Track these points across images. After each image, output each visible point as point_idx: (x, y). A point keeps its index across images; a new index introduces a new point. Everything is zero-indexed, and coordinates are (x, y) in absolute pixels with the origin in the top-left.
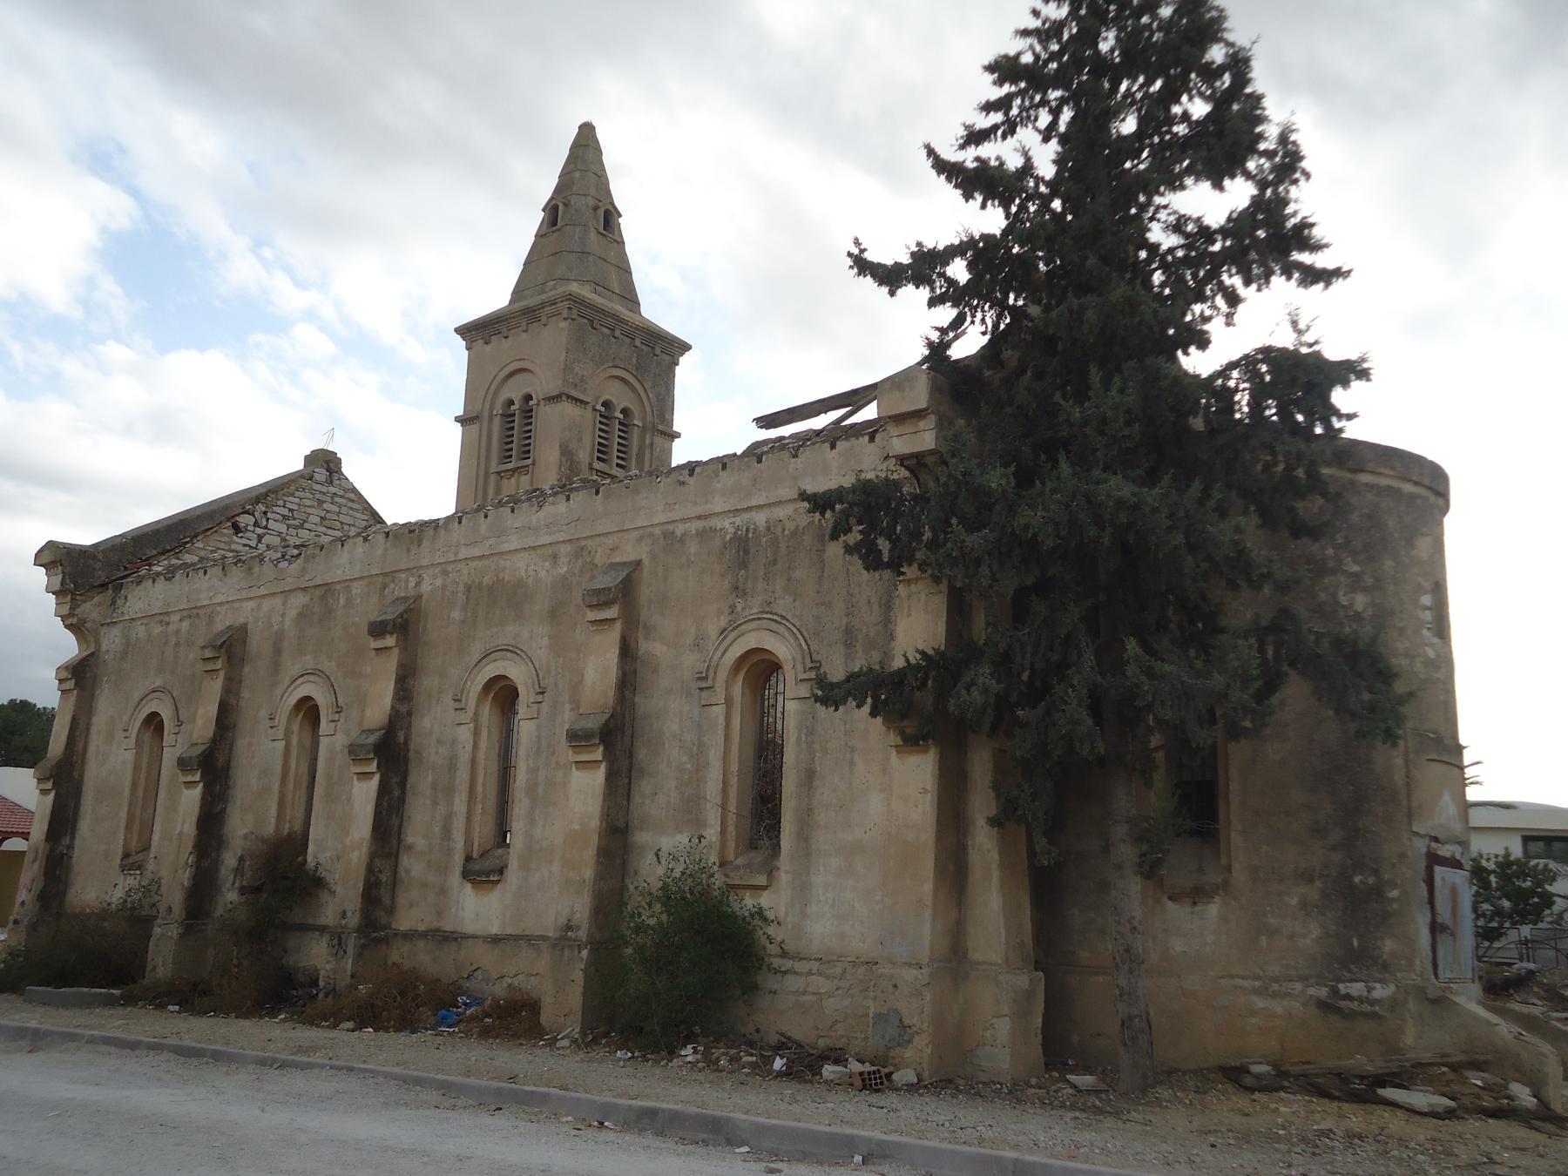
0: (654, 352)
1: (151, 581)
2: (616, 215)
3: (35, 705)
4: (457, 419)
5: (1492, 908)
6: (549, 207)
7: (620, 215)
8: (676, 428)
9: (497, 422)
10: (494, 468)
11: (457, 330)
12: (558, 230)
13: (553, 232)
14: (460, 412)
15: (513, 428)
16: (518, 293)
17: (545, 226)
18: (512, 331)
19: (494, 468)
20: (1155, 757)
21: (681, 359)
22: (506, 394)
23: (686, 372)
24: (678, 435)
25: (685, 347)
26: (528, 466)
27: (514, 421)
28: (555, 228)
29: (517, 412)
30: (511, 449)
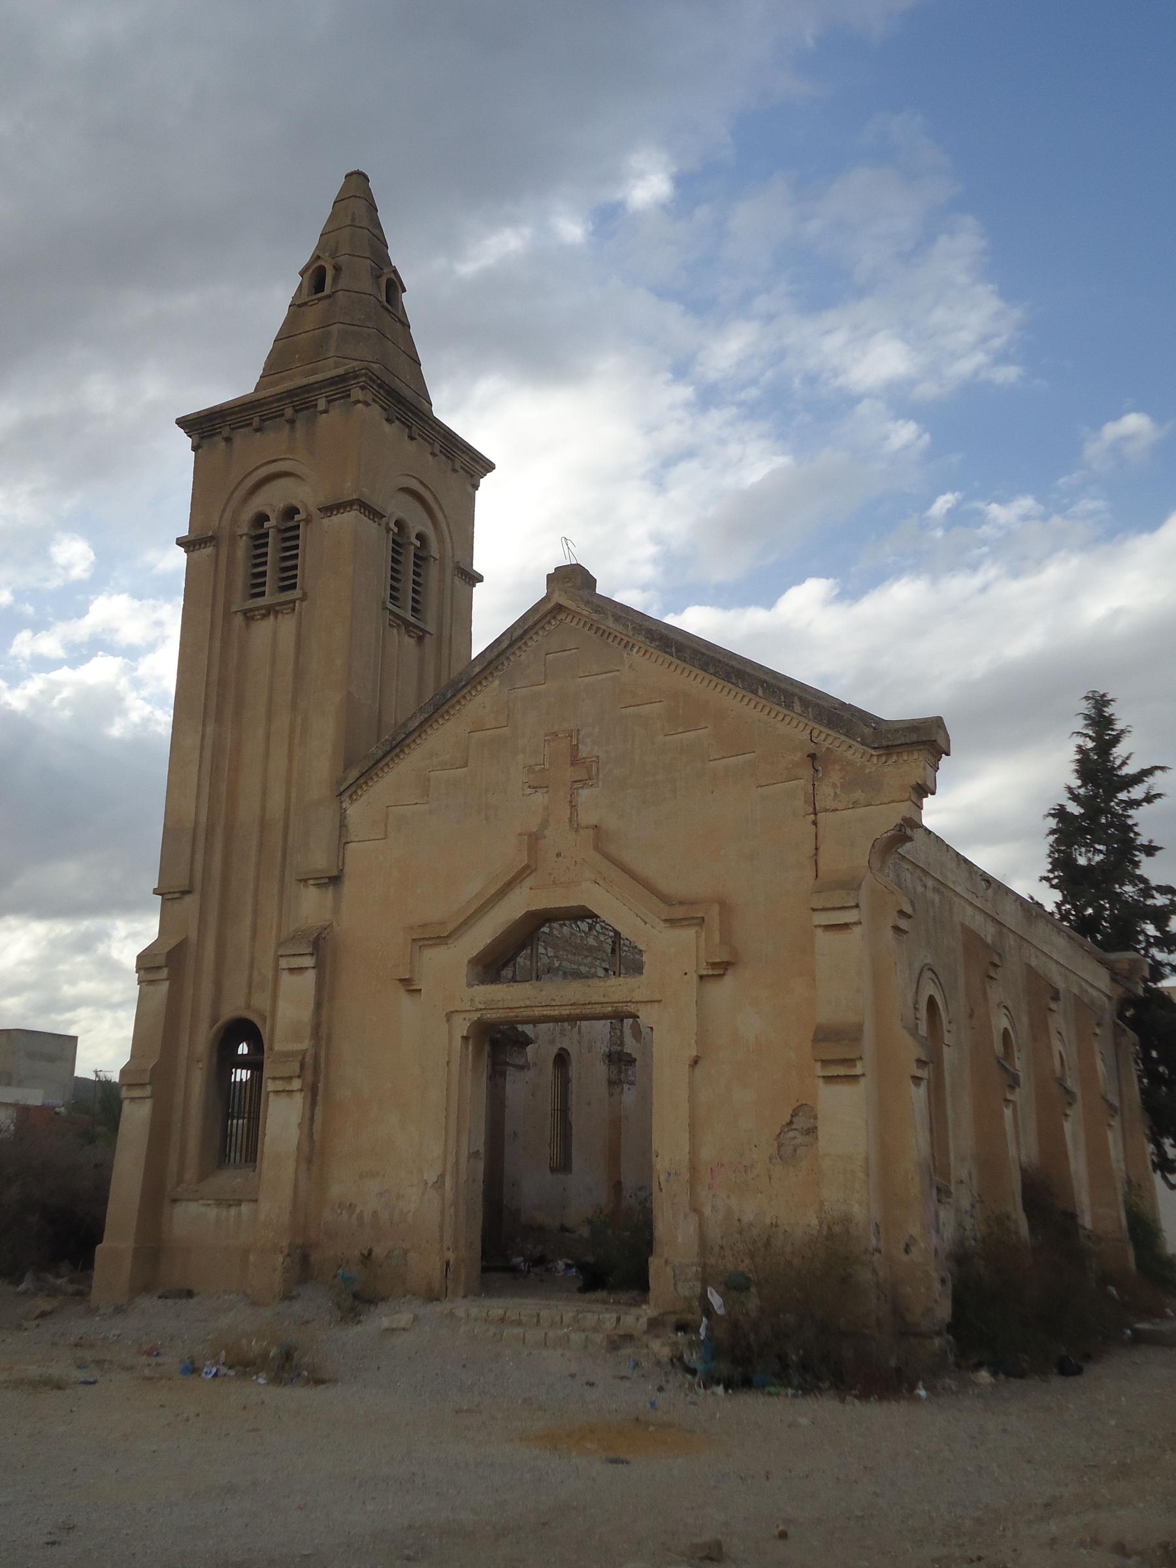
0: (453, 466)
1: (924, 1059)
2: (400, 290)
3: (1078, 805)
4: (181, 542)
5: (1158, 934)
6: (313, 268)
7: (404, 290)
8: (478, 566)
9: (243, 543)
10: (239, 604)
11: (183, 423)
12: (329, 297)
13: (319, 299)
14: (184, 532)
15: (264, 574)
16: (276, 365)
17: (305, 291)
18: (268, 422)
19: (239, 604)
20: (308, 948)
21: (482, 481)
22: (259, 503)
23: (487, 493)
24: (480, 579)
25: (489, 467)
26: (294, 601)
27: (266, 554)
28: (320, 295)
29: (271, 531)
30: (264, 574)
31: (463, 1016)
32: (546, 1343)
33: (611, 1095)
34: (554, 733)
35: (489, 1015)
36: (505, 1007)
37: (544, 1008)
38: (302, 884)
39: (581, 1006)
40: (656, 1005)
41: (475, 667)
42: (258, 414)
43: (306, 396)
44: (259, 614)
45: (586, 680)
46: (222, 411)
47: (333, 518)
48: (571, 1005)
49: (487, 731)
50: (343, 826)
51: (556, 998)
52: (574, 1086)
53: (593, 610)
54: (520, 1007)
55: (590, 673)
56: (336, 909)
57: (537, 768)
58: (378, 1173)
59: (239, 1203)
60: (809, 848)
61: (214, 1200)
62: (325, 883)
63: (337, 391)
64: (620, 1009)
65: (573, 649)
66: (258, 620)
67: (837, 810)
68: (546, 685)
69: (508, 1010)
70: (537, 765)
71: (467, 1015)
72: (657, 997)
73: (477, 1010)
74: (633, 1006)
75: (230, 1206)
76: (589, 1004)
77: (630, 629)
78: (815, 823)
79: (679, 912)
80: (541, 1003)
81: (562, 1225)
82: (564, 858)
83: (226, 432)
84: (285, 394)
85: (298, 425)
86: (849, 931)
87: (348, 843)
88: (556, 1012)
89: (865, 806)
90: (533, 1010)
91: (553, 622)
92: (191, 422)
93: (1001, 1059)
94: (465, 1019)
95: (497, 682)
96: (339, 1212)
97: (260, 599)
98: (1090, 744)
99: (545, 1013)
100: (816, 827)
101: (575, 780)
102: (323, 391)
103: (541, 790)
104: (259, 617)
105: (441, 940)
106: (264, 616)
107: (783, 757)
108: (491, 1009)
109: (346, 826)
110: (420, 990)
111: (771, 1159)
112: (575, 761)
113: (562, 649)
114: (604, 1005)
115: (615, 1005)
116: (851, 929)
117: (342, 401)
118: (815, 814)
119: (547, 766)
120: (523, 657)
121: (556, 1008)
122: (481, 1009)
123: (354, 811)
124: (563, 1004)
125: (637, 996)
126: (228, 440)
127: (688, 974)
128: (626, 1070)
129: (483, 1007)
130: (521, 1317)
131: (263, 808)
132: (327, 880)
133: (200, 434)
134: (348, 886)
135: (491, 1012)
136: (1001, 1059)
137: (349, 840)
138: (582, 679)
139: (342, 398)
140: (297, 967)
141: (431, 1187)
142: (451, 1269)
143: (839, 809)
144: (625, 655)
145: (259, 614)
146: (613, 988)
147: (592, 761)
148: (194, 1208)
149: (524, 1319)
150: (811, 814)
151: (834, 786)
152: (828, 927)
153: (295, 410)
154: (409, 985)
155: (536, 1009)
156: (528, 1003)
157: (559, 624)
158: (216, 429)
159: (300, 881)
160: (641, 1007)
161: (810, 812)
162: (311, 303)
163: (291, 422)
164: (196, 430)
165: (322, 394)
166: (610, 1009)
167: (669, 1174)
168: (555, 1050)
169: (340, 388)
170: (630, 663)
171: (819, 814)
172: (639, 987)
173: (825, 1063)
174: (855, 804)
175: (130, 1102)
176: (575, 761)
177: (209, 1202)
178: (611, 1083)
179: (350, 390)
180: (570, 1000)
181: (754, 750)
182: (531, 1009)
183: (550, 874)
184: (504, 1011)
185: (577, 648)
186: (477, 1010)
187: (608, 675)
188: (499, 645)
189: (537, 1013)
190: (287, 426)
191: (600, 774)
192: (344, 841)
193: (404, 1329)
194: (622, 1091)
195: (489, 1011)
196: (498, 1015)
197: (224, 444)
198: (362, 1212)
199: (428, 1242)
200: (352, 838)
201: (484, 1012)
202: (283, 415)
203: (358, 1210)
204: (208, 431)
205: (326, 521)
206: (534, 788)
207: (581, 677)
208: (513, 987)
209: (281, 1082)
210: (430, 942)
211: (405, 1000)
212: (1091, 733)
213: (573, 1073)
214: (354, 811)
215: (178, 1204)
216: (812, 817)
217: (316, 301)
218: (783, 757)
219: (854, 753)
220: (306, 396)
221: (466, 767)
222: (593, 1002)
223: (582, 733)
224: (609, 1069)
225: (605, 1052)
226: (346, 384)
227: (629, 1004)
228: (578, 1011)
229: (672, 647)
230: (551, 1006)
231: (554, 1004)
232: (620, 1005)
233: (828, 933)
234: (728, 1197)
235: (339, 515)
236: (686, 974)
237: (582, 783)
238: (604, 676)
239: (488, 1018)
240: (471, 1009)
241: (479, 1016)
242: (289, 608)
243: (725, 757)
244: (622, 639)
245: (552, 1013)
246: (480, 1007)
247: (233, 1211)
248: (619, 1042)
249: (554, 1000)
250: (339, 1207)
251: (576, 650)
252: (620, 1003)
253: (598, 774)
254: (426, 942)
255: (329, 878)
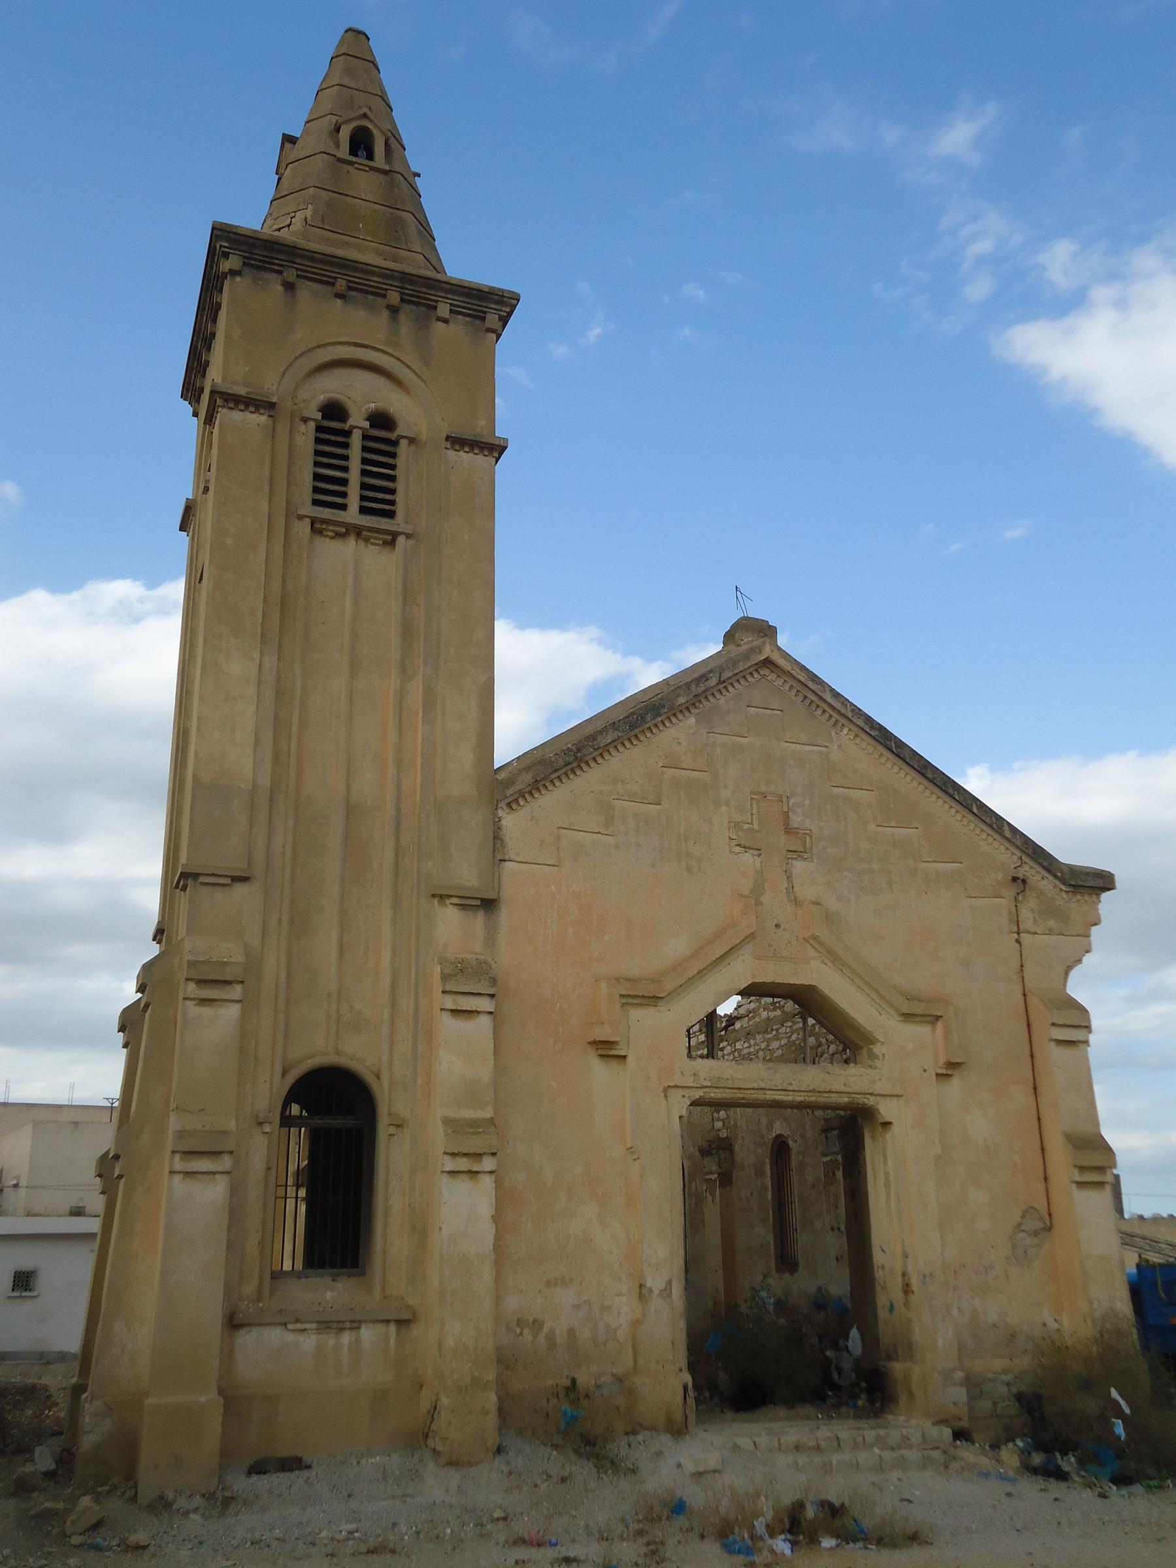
31: (681, 1092)
32: (881, 1468)
34: (763, 793)
35: (712, 1095)
36: (735, 1086)
37: (778, 1092)
38: (436, 900)
39: (817, 1094)
40: (895, 1100)
41: (679, 696)
42: (348, 278)
43: (424, 290)
44: (332, 531)
45: (793, 746)
46: (295, 247)
47: (461, 454)
48: (810, 1091)
49: (684, 771)
50: (497, 837)
51: (793, 1082)
53: (809, 678)
54: (753, 1089)
55: (798, 740)
56: (491, 940)
57: (746, 827)
58: (572, 1280)
59: (356, 1325)
60: (1015, 963)
61: (317, 1322)
62: (477, 906)
63: (467, 305)
64: (856, 1100)
65: (776, 710)
66: (327, 536)
67: (1037, 934)
68: (747, 740)
69: (737, 1091)
70: (746, 823)
71: (686, 1092)
72: (898, 1091)
73: (703, 1087)
74: (872, 1098)
75: (342, 1329)
76: (829, 1092)
77: (849, 710)
78: (1018, 941)
79: (918, 1009)
80: (776, 1086)
82: (785, 930)
83: (290, 275)
84: (396, 274)
85: (402, 317)
86: (1076, 1048)
87: (504, 861)
88: (790, 1098)
89: (1057, 935)
90: (765, 1094)
91: (756, 675)
92: (466, 290)
94: (684, 1096)
95: (692, 720)
96: (518, 1331)
97: (383, 520)
99: (777, 1097)
100: (1021, 946)
101: (790, 849)
102: (449, 296)
103: (752, 851)
104: (331, 534)
105: (653, 1000)
106: (338, 535)
107: (988, 874)
108: (717, 1088)
109: (502, 840)
110: (625, 1057)
111: (1007, 1258)
112: (788, 830)
113: (765, 707)
114: (842, 1095)
115: (853, 1096)
116: (1077, 1046)
117: (468, 319)
118: (1018, 934)
119: (756, 827)
120: (722, 702)
121: (791, 1093)
122: (706, 1087)
123: (511, 822)
124: (801, 1089)
125: (879, 1088)
126: (289, 286)
127: (927, 1072)
129: (709, 1085)
130: (819, 1443)
131: (348, 788)
132: (478, 903)
133: (244, 257)
134: (505, 914)
135: (717, 1091)
137: (507, 857)
138: (787, 744)
139: (469, 315)
140: (469, 1009)
141: (657, 1296)
142: (690, 1393)
143: (1038, 932)
144: (833, 734)
145: (332, 531)
146: (854, 1078)
147: (806, 834)
148: (274, 1336)
149: (823, 1444)
150: (1015, 933)
151: (1033, 911)
152: (1060, 1042)
153: (401, 298)
154: (607, 1050)
155: (767, 1092)
156: (762, 1085)
157: (761, 679)
158: (274, 264)
159: (434, 896)
160: (881, 1100)
161: (1014, 931)
162: (359, 167)
163: (394, 310)
164: (240, 251)
165: (447, 298)
166: (846, 1099)
167: (924, 1276)
169: (472, 304)
170: (839, 743)
171: (1021, 934)
172: (880, 1080)
173: (1082, 1169)
174: (1050, 932)
175: (183, 1179)
176: (788, 830)
177: (306, 1326)
179: (485, 313)
180: (808, 1086)
181: (962, 861)
182: (762, 1092)
183: (770, 945)
184: (732, 1091)
185: (782, 711)
186: (703, 1087)
187: (815, 748)
188: (705, 681)
189: (768, 1097)
190: (386, 314)
191: (814, 849)
192: (500, 857)
193: (714, 1471)
195: (714, 1090)
196: (724, 1095)
197: (280, 288)
198: (552, 1331)
199: (658, 1362)
200: (512, 857)
201: (708, 1090)
202: (333, 284)
203: (546, 1329)
204: (260, 261)
205: (451, 454)
206: (744, 847)
207: (786, 742)
208: (743, 1065)
209: (465, 1160)
210: (635, 1001)
211: (599, 1070)
214: (511, 822)
215: (242, 1331)
216: (1016, 935)
217: (368, 169)
218: (988, 874)
219: (1045, 884)
220: (424, 290)
221: (660, 805)
222: (834, 1090)
223: (792, 801)
226: (484, 304)
227: (868, 1096)
228: (813, 1099)
229: (891, 740)
230: (786, 1090)
231: (791, 1088)
232: (858, 1096)
233: (1059, 1047)
234: (973, 1298)
235: (471, 455)
236: (925, 1071)
237: (797, 853)
238: (810, 748)
239: (711, 1098)
240: (695, 1085)
241: (702, 1094)
242: (381, 539)
243: (936, 862)
244: (837, 721)
245: (785, 1098)
246: (705, 1085)
247: (346, 1338)
249: (791, 1084)
250: (518, 1324)
251: (779, 712)
252: (857, 1094)
253: (812, 847)
254: (630, 1000)
255: (482, 900)
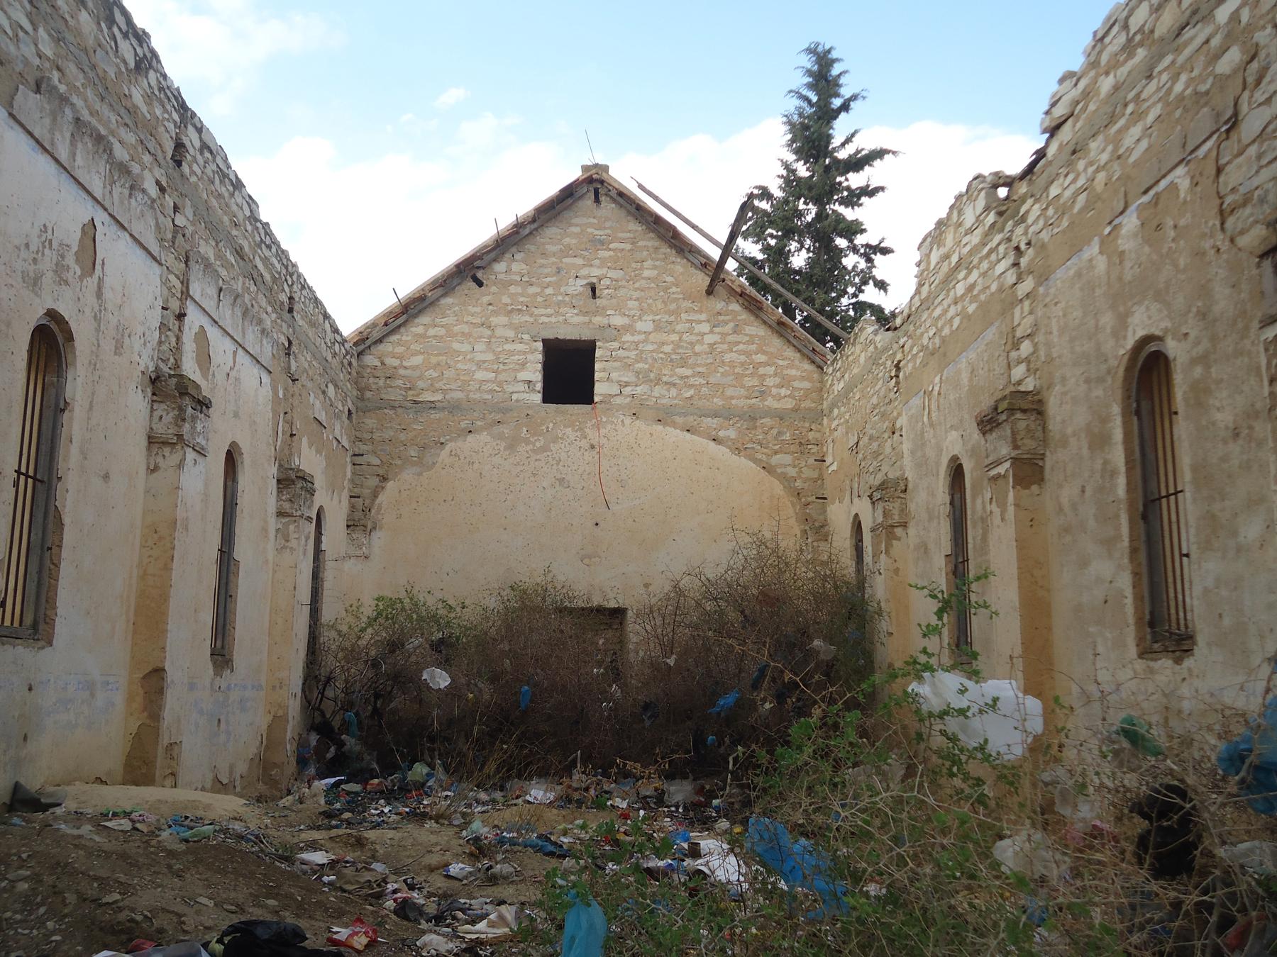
33: (153, 470)
52: (75, 425)
81: (17, 787)
93: (1128, 35)
98: (809, 110)
128: (194, 419)
136: (1128, 35)
168: (35, 316)
178: (153, 441)
194: (180, 465)
212: (814, 99)
213: (77, 385)
224: (152, 410)
225: (147, 367)
248: (172, 360)
